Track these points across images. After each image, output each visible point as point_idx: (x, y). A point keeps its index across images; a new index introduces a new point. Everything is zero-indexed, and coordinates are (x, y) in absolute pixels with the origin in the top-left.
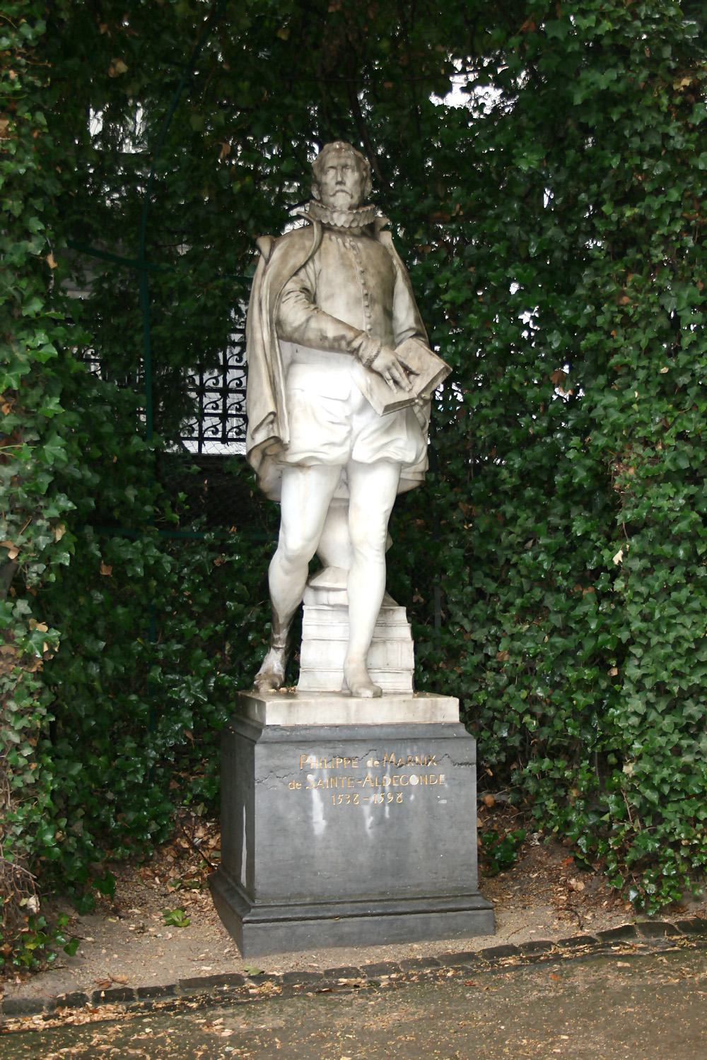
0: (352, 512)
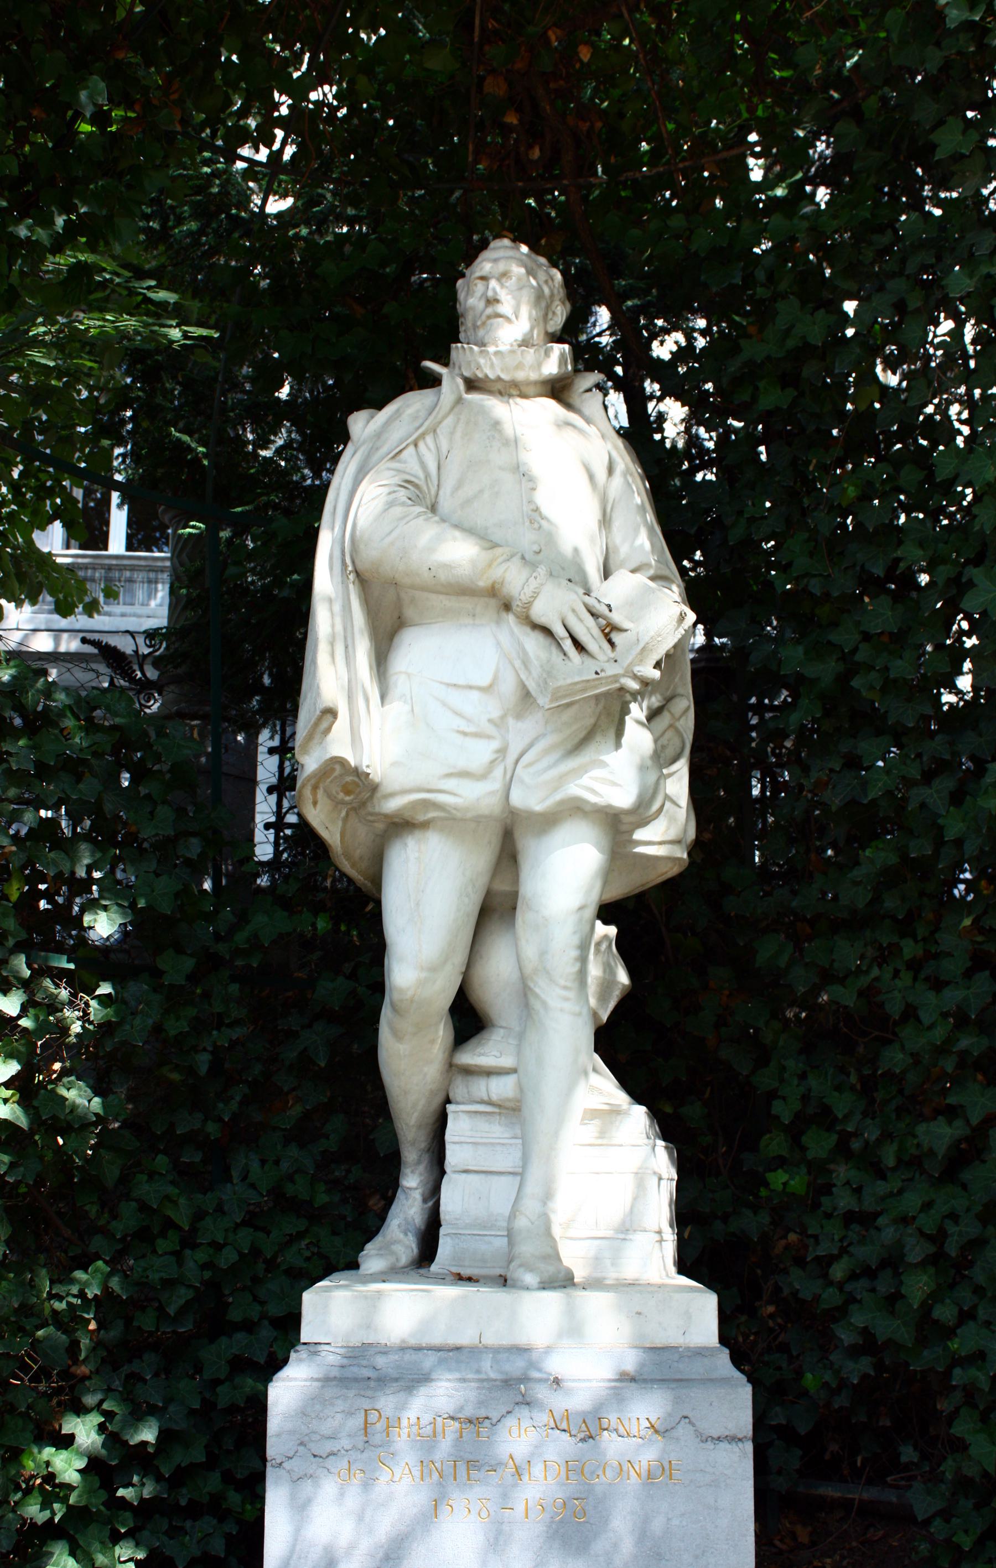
0: (523, 917)
